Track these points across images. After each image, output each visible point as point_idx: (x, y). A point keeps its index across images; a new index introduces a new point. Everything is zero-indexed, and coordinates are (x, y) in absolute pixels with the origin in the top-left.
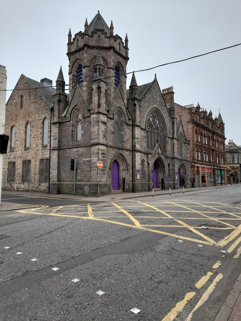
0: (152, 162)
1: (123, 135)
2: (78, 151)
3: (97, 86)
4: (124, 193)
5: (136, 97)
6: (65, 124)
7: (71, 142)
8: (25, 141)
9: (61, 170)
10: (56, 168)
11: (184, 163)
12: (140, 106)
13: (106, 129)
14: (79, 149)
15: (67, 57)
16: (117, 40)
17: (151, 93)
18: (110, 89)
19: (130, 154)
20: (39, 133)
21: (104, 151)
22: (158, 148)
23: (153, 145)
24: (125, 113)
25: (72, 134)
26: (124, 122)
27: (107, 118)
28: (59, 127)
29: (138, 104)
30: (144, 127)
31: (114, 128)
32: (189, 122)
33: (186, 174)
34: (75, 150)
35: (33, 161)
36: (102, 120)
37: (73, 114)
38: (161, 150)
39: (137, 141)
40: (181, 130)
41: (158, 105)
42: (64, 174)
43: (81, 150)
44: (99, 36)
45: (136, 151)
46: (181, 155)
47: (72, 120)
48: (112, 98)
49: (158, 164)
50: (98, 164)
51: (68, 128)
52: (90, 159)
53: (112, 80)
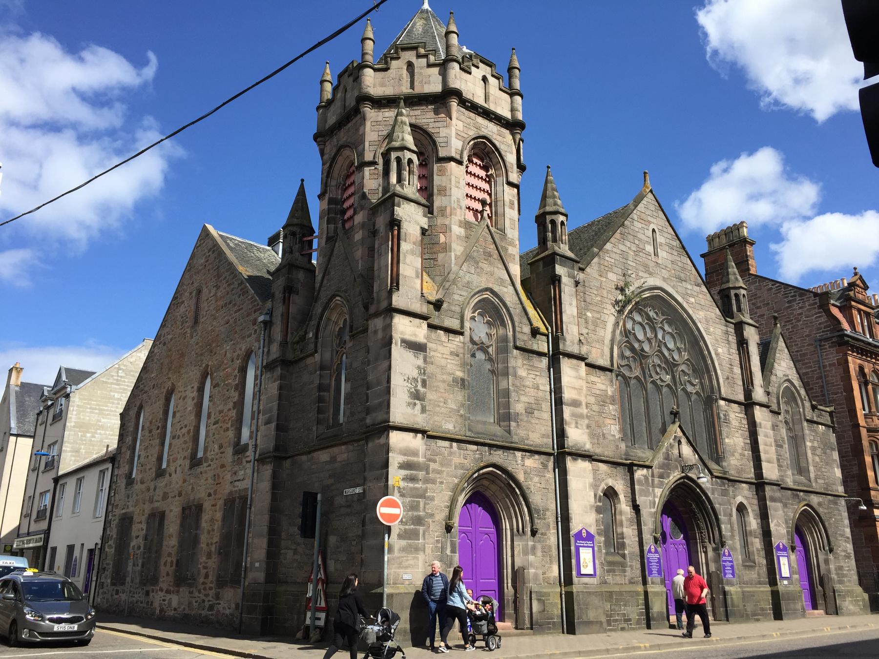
0: (653, 499)
1: (507, 394)
2: (333, 459)
3: (388, 219)
4: (717, 624)
5: (744, 319)
6: (302, 364)
7: (315, 428)
8: (194, 435)
9: (283, 535)
10: (265, 529)
11: (815, 506)
12: (577, 283)
13: (422, 371)
14: (336, 450)
15: (315, 148)
16: (473, 69)
17: (631, 238)
18: (446, 229)
19: (545, 466)
20: (231, 405)
21: (415, 453)
22: (680, 442)
23: (656, 430)
24: (516, 311)
25: (320, 400)
26: (512, 344)
27: (430, 326)
28: (282, 377)
29: (571, 276)
30: (604, 362)
31: (463, 365)
32: (826, 339)
33: (831, 550)
34: (323, 456)
35: (207, 505)
36: (408, 337)
37: (325, 329)
38: (695, 450)
39: (573, 415)
40: (788, 372)
41: (664, 279)
42: (290, 553)
43: (342, 454)
44: (410, 65)
45: (570, 454)
46: (801, 469)
47: (319, 351)
48: (457, 257)
49: (687, 510)
50: (382, 505)
51: (308, 378)
52: (358, 490)
53: (453, 198)
